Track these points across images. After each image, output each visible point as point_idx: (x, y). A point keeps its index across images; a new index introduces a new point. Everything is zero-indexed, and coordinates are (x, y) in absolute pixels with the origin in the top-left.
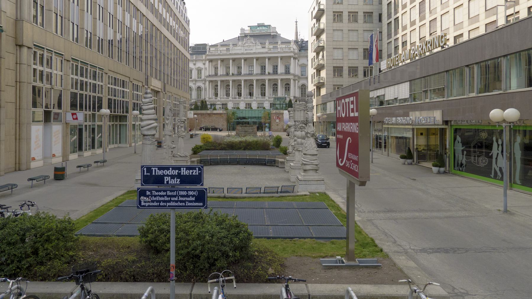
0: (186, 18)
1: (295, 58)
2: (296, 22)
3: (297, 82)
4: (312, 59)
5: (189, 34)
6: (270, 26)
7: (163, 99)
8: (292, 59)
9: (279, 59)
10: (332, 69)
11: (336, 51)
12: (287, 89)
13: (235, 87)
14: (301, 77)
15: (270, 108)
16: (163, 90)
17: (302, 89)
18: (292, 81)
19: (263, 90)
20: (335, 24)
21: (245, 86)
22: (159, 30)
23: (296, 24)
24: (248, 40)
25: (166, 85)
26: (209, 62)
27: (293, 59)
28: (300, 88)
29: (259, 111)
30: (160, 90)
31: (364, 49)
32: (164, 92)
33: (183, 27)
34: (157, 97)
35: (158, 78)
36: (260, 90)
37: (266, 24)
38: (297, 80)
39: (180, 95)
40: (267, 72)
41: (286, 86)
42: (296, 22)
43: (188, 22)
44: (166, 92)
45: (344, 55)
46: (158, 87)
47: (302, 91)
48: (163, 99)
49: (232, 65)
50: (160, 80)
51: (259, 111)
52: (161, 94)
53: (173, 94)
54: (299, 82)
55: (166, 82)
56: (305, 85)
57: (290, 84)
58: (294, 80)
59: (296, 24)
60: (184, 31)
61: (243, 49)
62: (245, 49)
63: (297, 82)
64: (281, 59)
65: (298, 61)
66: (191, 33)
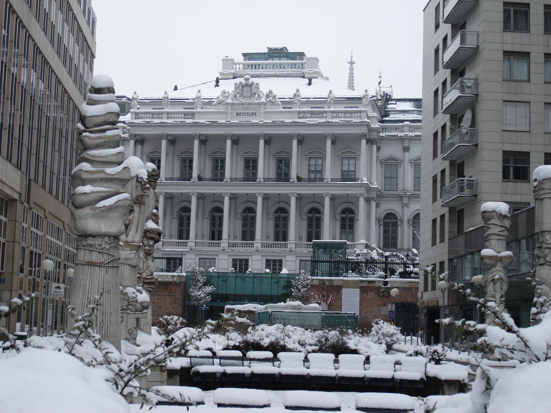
0: (89, 11)
1: (370, 142)
2: (352, 63)
3: (374, 204)
4: (436, 134)
5: (93, 56)
6: (301, 55)
7: (24, 224)
8: (364, 142)
9: (329, 142)
10: (500, 157)
11: (510, 108)
12: (347, 223)
13: (204, 215)
14: (385, 193)
15: (300, 269)
16: (23, 199)
17: (386, 225)
18: (362, 202)
19: (281, 226)
20: (509, 36)
21: (233, 214)
22: (24, 27)
23: (351, 69)
24: (245, 89)
25: (33, 184)
26: (135, 144)
27: (367, 143)
28: (382, 223)
29: (274, 280)
30: (16, 196)
31: (505, 153)
32: (26, 204)
33: (81, 34)
34: (6, 216)
35: (15, 160)
36: (272, 224)
37: (290, 50)
38: (373, 199)
39: (63, 219)
40: (293, 174)
41: (344, 215)
42: (352, 63)
43: (92, 22)
44: (32, 205)
45: (532, 121)
46: (14, 186)
47: (385, 232)
48: (24, 224)
49: (199, 154)
50: (18, 166)
51: (274, 280)
52: (20, 207)
53: (47, 214)
54: (378, 205)
55: (32, 176)
56: (396, 218)
57: (356, 211)
58: (368, 200)
59: (351, 69)
60: (43, 71)
61: (229, 111)
62: (235, 112)
63: (374, 204)
64: (333, 143)
65: (378, 149)
66: (98, 54)
